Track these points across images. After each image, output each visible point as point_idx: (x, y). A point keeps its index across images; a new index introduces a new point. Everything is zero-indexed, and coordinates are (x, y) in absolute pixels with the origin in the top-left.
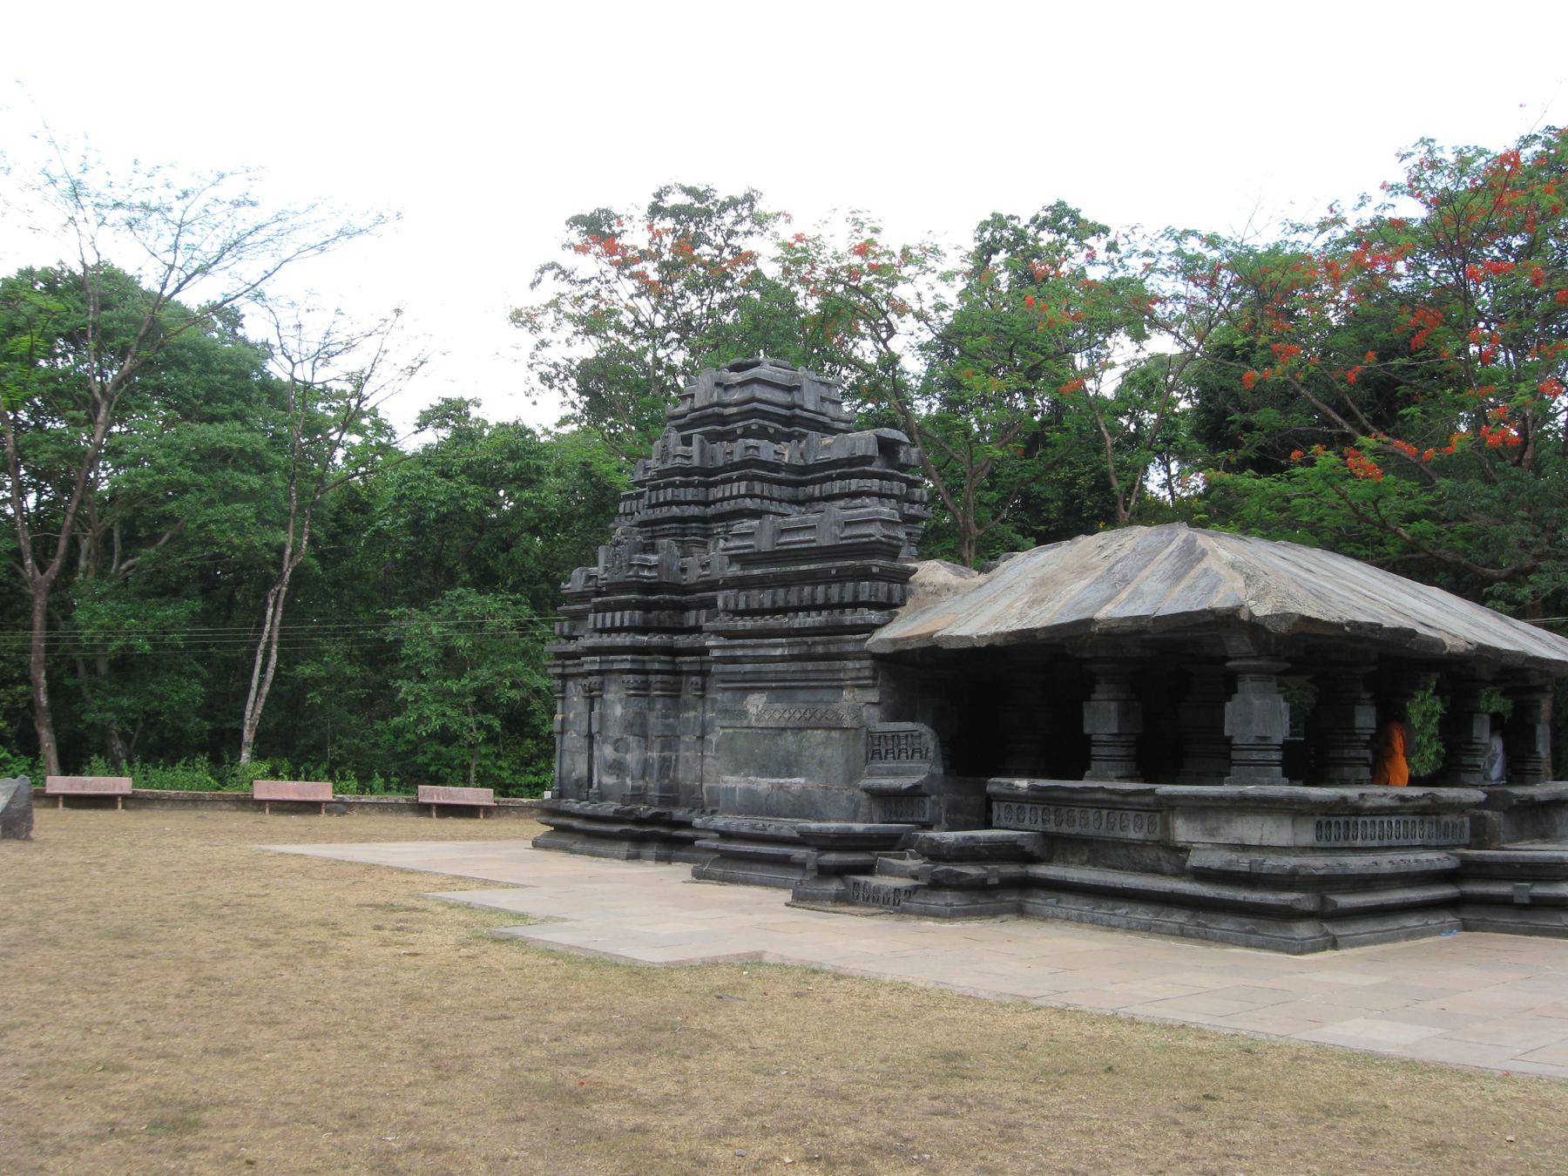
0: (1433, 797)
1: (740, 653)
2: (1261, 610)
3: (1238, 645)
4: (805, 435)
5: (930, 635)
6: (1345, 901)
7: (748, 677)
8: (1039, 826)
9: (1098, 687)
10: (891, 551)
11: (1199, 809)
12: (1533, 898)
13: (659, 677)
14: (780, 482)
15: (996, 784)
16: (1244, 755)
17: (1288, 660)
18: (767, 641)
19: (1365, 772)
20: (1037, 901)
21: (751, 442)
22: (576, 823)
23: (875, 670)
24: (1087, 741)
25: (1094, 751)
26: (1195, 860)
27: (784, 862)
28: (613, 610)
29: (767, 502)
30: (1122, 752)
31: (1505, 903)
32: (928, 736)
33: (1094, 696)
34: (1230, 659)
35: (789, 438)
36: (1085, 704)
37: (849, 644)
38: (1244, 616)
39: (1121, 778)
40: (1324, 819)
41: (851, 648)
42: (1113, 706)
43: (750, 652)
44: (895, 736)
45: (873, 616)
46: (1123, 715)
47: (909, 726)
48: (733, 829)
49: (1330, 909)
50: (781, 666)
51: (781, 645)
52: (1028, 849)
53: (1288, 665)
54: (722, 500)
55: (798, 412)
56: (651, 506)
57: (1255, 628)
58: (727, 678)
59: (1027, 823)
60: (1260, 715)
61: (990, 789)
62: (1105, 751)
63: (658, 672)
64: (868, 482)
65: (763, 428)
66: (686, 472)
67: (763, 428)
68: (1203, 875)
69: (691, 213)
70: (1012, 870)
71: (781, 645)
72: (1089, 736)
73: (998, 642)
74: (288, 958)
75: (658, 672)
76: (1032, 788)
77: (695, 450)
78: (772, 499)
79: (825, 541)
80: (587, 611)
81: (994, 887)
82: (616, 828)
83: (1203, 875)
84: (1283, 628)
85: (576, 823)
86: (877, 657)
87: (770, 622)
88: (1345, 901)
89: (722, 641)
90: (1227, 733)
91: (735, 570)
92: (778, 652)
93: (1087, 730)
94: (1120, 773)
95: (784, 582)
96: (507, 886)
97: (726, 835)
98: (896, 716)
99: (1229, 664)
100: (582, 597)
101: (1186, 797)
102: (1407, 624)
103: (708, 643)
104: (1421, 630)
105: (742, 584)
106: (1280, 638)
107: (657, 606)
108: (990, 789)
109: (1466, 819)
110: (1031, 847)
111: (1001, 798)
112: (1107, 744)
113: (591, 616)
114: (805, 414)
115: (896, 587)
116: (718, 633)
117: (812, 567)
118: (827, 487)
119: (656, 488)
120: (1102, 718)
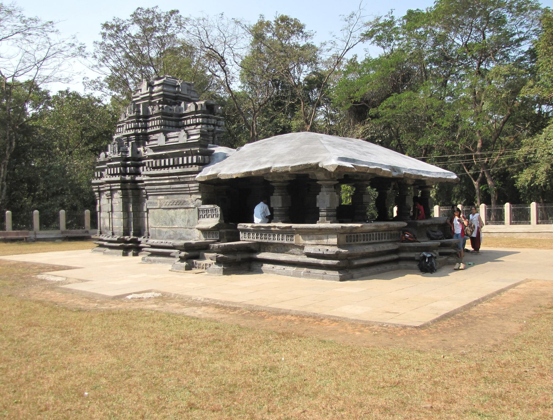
0: (389, 226)
1: (154, 182)
5: (216, 175)
9: (275, 191)
11: (306, 233)
14: (172, 120)
15: (241, 226)
17: (338, 180)
20: (402, 264)
22: (105, 243)
23: (199, 187)
26: (308, 249)
27: (168, 255)
29: (171, 128)
30: (282, 213)
32: (219, 210)
33: (274, 194)
34: (318, 180)
35: (175, 104)
36: (271, 197)
37: (190, 178)
41: (191, 179)
44: (207, 210)
45: (195, 168)
46: (283, 201)
47: (212, 206)
48: (154, 244)
50: (169, 186)
56: (127, 130)
68: (309, 255)
69: (147, 21)
72: (318, 208)
73: (239, 176)
74: (522, 302)
78: (169, 126)
80: (106, 168)
82: (118, 245)
83: (309, 255)
85: (105, 243)
86: (201, 182)
89: (148, 178)
90: (317, 206)
91: (152, 153)
95: (173, 155)
96: (79, 268)
97: (153, 247)
98: (204, 203)
99: (318, 182)
100: (103, 163)
101: (302, 229)
103: (143, 179)
105: (154, 157)
108: (238, 227)
113: (106, 170)
114: (184, 96)
115: (207, 157)
116: (147, 175)
119: (128, 123)
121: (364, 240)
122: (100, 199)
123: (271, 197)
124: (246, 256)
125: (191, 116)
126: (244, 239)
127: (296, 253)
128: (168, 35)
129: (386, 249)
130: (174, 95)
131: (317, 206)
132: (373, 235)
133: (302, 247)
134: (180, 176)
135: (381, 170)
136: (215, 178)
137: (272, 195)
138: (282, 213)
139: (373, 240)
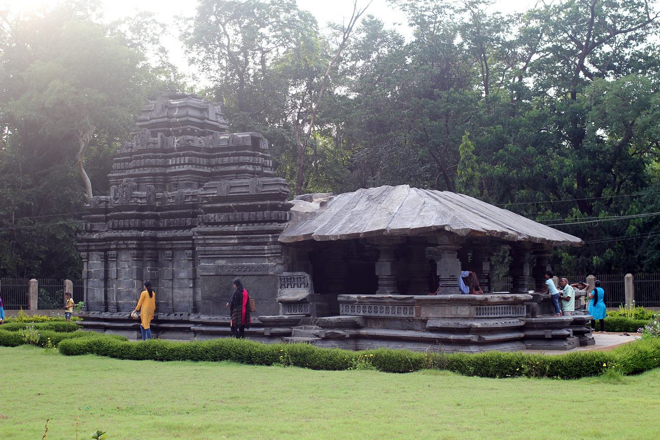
2: (455, 228)
3: (445, 239)
4: (212, 133)
6: (488, 338)
7: (216, 252)
8: (362, 313)
10: (281, 196)
12: (552, 335)
13: (149, 251)
15: (342, 297)
16: (444, 283)
17: (461, 245)
18: (226, 237)
19: (486, 288)
21: (190, 137)
24: (377, 279)
25: (380, 282)
26: (430, 324)
28: (119, 219)
30: (392, 282)
31: (542, 338)
32: (308, 278)
33: (379, 260)
36: (376, 263)
38: (447, 229)
39: (391, 293)
40: (478, 307)
42: (388, 264)
43: (217, 241)
49: (482, 341)
51: (234, 239)
52: (358, 323)
53: (461, 247)
54: (175, 165)
55: (207, 121)
57: (451, 234)
58: (205, 253)
59: (356, 312)
60: (449, 266)
61: (339, 299)
62: (385, 282)
63: (149, 249)
64: (248, 158)
65: (184, 130)
66: (155, 151)
67: (193, 130)
68: (433, 330)
70: (353, 332)
71: (234, 239)
72: (377, 276)
75: (149, 249)
76: (359, 298)
77: (158, 139)
79: (252, 192)
81: (348, 339)
83: (433, 330)
84: (464, 234)
87: (226, 228)
88: (488, 338)
90: (438, 274)
92: (232, 241)
93: (377, 274)
94: (392, 291)
102: (499, 229)
104: (510, 232)
106: (462, 238)
107: (147, 217)
108: (339, 299)
109: (525, 306)
110: (360, 322)
111: (342, 302)
112: (387, 279)
117: (248, 204)
118: (226, 160)
120: (384, 269)
121: (491, 314)
122: (87, 262)
123: (376, 263)
124: (353, 332)
125: (230, 153)
126: (345, 313)
127: (31, 333)
128: (553, 42)
129: (512, 325)
130: (199, 121)
131: (438, 274)
132: (499, 308)
133: (425, 321)
134: (205, 237)
135: (507, 233)
136: (308, 239)
137: (377, 261)
138: (392, 282)
139: (486, 314)
